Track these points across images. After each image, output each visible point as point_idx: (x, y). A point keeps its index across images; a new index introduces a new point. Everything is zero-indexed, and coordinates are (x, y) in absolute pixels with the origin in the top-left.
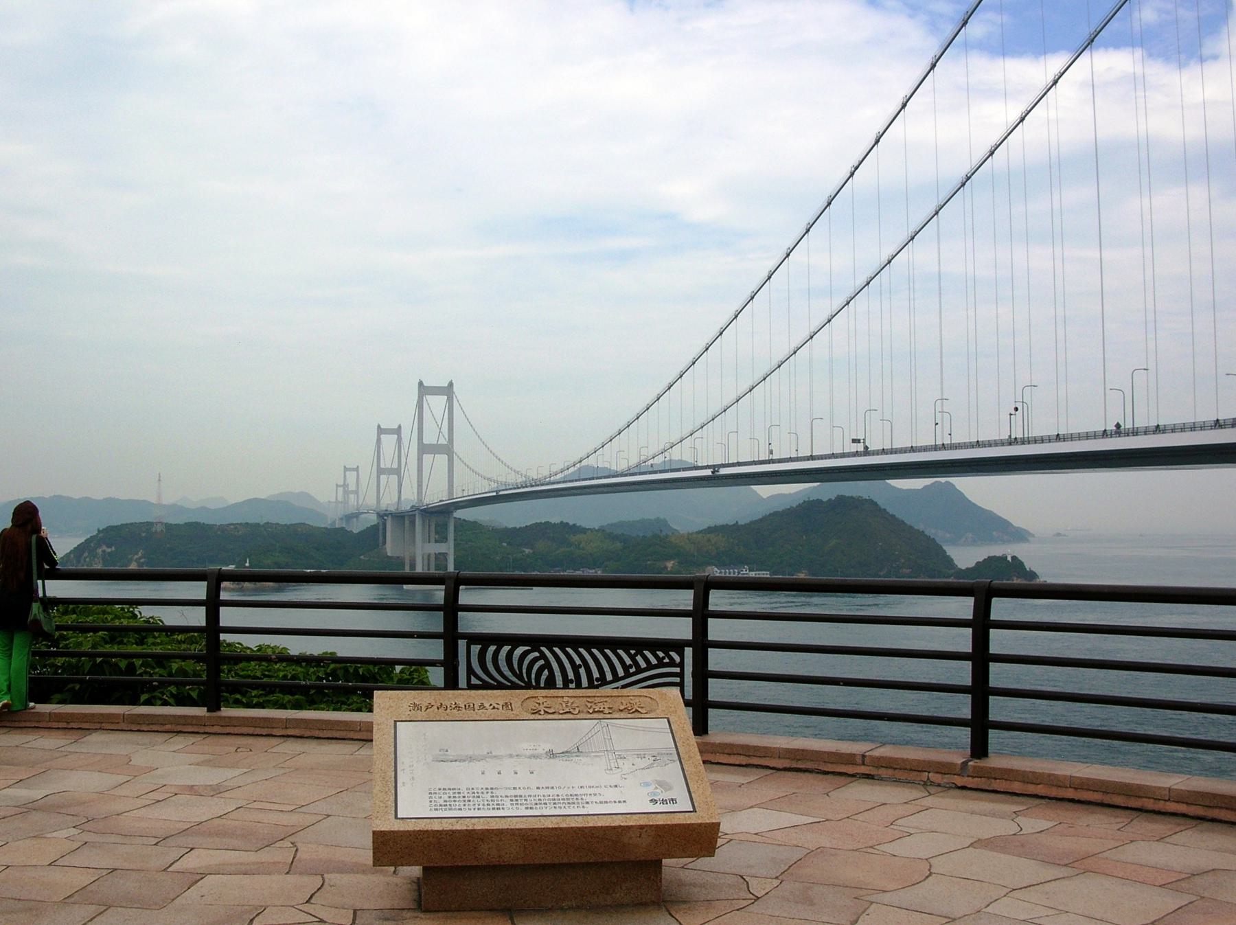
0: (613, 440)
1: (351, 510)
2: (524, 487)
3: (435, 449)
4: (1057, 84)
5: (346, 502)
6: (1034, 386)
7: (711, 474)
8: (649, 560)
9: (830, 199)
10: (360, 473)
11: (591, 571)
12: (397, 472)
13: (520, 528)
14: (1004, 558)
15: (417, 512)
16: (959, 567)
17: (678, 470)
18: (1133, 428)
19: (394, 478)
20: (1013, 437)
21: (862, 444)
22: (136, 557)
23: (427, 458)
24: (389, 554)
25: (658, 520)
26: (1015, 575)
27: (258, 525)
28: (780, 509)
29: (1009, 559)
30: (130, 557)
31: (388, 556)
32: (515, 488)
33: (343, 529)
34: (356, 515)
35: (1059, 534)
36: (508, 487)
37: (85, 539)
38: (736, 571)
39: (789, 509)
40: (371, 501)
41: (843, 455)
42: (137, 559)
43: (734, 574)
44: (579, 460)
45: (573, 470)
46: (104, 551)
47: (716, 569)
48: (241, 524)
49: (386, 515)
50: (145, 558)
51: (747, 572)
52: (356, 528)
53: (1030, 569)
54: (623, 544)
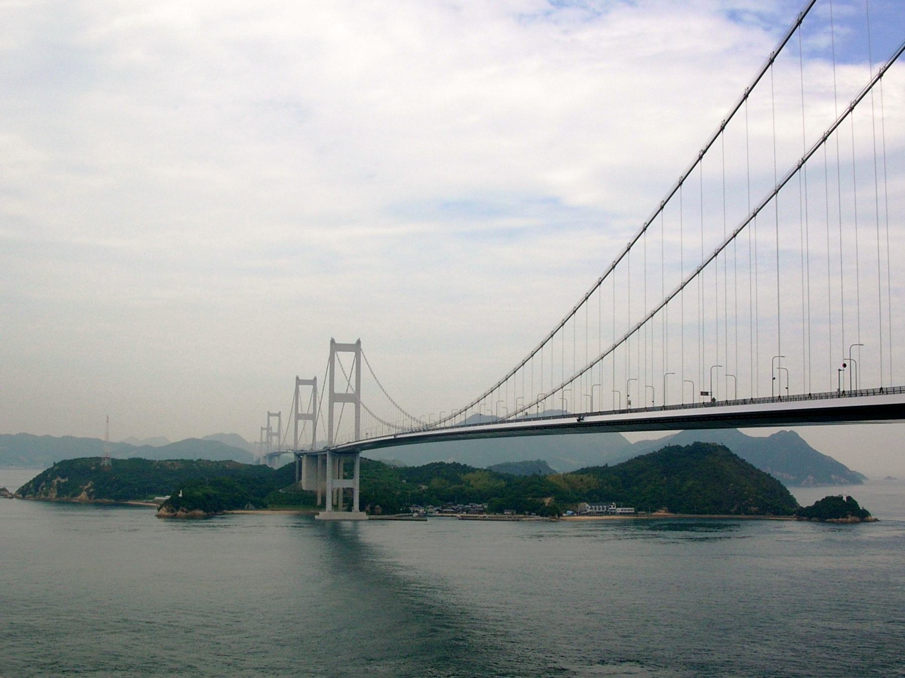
0: (494, 391)
1: (273, 449)
2: (418, 432)
3: (344, 398)
4: (883, 78)
5: (268, 443)
6: (720, 366)
7: (576, 421)
8: (529, 497)
9: (682, 179)
10: (282, 419)
11: (478, 506)
12: (313, 417)
13: (418, 467)
14: (840, 498)
15: (327, 453)
16: (801, 505)
17: (549, 418)
18: (851, 391)
19: (310, 423)
20: (841, 390)
21: (710, 396)
22: (86, 487)
23: (338, 406)
24: (304, 489)
25: (538, 462)
26: (849, 514)
27: (191, 461)
28: (644, 454)
29: (845, 499)
30: (81, 487)
31: (303, 490)
32: (410, 433)
33: (265, 466)
34: (277, 455)
35: (889, 478)
36: (405, 432)
37: (43, 471)
38: (605, 507)
39: (652, 454)
40: (290, 442)
41: (693, 406)
42: (87, 489)
43: (603, 509)
44: (464, 409)
45: (522, 415)
46: (58, 482)
47: (587, 505)
48: (177, 460)
49: (302, 454)
50: (94, 488)
51: (615, 508)
52: (277, 465)
53: (863, 508)
54: (506, 482)
